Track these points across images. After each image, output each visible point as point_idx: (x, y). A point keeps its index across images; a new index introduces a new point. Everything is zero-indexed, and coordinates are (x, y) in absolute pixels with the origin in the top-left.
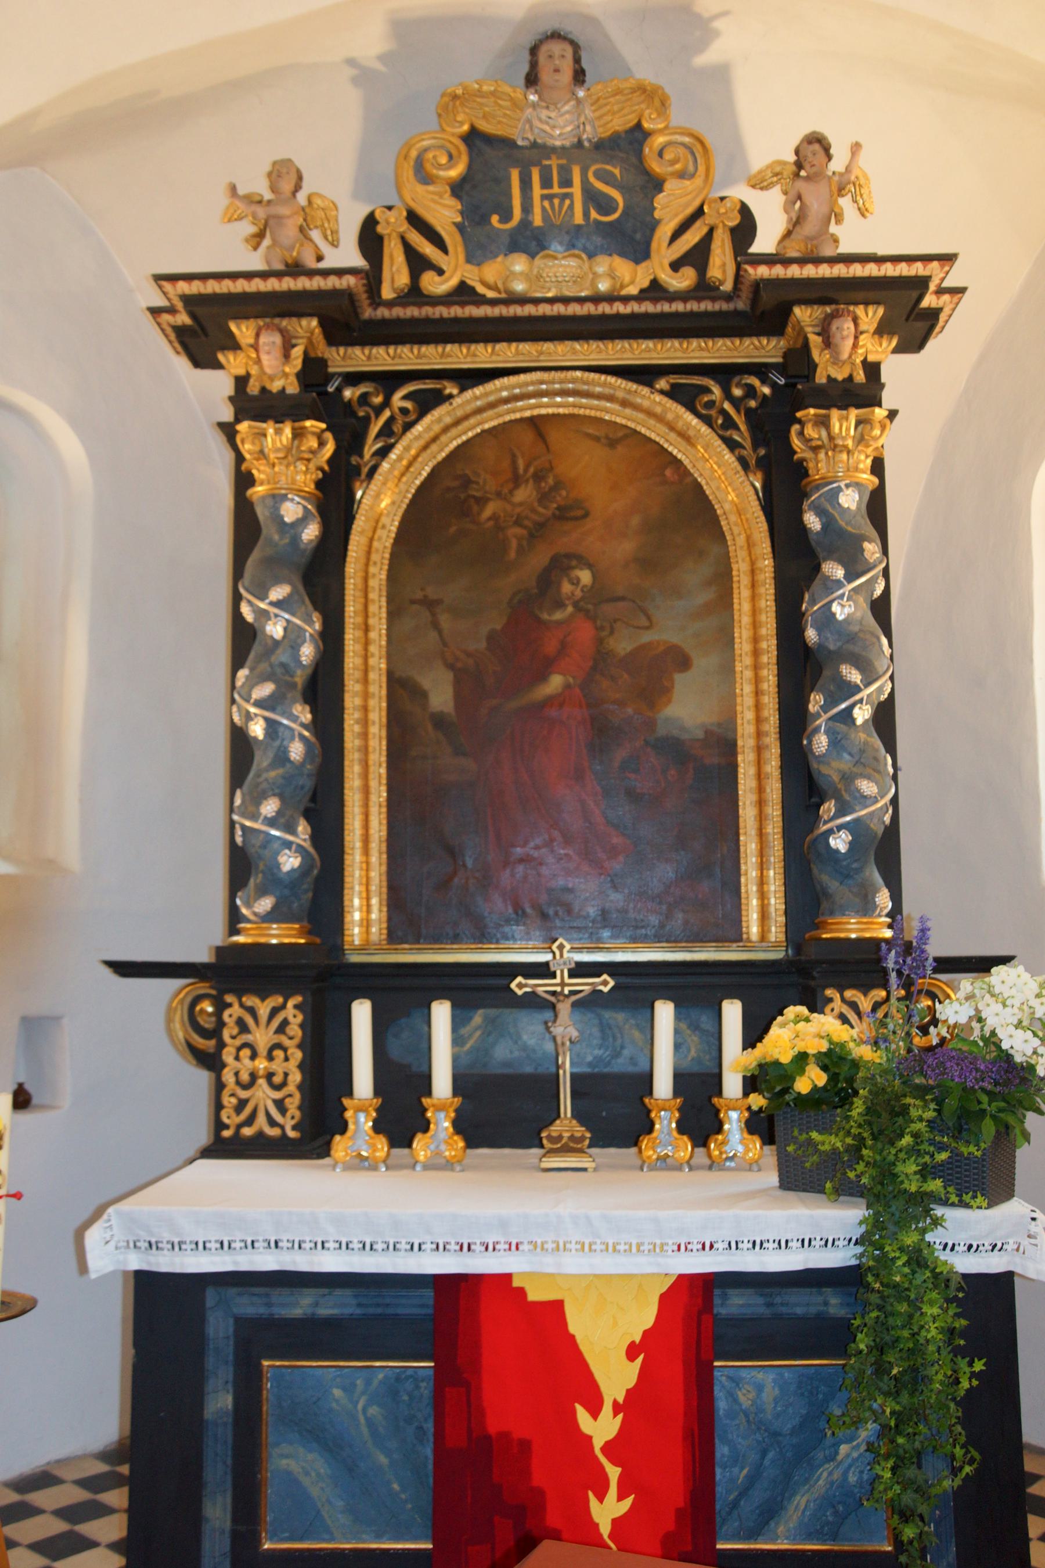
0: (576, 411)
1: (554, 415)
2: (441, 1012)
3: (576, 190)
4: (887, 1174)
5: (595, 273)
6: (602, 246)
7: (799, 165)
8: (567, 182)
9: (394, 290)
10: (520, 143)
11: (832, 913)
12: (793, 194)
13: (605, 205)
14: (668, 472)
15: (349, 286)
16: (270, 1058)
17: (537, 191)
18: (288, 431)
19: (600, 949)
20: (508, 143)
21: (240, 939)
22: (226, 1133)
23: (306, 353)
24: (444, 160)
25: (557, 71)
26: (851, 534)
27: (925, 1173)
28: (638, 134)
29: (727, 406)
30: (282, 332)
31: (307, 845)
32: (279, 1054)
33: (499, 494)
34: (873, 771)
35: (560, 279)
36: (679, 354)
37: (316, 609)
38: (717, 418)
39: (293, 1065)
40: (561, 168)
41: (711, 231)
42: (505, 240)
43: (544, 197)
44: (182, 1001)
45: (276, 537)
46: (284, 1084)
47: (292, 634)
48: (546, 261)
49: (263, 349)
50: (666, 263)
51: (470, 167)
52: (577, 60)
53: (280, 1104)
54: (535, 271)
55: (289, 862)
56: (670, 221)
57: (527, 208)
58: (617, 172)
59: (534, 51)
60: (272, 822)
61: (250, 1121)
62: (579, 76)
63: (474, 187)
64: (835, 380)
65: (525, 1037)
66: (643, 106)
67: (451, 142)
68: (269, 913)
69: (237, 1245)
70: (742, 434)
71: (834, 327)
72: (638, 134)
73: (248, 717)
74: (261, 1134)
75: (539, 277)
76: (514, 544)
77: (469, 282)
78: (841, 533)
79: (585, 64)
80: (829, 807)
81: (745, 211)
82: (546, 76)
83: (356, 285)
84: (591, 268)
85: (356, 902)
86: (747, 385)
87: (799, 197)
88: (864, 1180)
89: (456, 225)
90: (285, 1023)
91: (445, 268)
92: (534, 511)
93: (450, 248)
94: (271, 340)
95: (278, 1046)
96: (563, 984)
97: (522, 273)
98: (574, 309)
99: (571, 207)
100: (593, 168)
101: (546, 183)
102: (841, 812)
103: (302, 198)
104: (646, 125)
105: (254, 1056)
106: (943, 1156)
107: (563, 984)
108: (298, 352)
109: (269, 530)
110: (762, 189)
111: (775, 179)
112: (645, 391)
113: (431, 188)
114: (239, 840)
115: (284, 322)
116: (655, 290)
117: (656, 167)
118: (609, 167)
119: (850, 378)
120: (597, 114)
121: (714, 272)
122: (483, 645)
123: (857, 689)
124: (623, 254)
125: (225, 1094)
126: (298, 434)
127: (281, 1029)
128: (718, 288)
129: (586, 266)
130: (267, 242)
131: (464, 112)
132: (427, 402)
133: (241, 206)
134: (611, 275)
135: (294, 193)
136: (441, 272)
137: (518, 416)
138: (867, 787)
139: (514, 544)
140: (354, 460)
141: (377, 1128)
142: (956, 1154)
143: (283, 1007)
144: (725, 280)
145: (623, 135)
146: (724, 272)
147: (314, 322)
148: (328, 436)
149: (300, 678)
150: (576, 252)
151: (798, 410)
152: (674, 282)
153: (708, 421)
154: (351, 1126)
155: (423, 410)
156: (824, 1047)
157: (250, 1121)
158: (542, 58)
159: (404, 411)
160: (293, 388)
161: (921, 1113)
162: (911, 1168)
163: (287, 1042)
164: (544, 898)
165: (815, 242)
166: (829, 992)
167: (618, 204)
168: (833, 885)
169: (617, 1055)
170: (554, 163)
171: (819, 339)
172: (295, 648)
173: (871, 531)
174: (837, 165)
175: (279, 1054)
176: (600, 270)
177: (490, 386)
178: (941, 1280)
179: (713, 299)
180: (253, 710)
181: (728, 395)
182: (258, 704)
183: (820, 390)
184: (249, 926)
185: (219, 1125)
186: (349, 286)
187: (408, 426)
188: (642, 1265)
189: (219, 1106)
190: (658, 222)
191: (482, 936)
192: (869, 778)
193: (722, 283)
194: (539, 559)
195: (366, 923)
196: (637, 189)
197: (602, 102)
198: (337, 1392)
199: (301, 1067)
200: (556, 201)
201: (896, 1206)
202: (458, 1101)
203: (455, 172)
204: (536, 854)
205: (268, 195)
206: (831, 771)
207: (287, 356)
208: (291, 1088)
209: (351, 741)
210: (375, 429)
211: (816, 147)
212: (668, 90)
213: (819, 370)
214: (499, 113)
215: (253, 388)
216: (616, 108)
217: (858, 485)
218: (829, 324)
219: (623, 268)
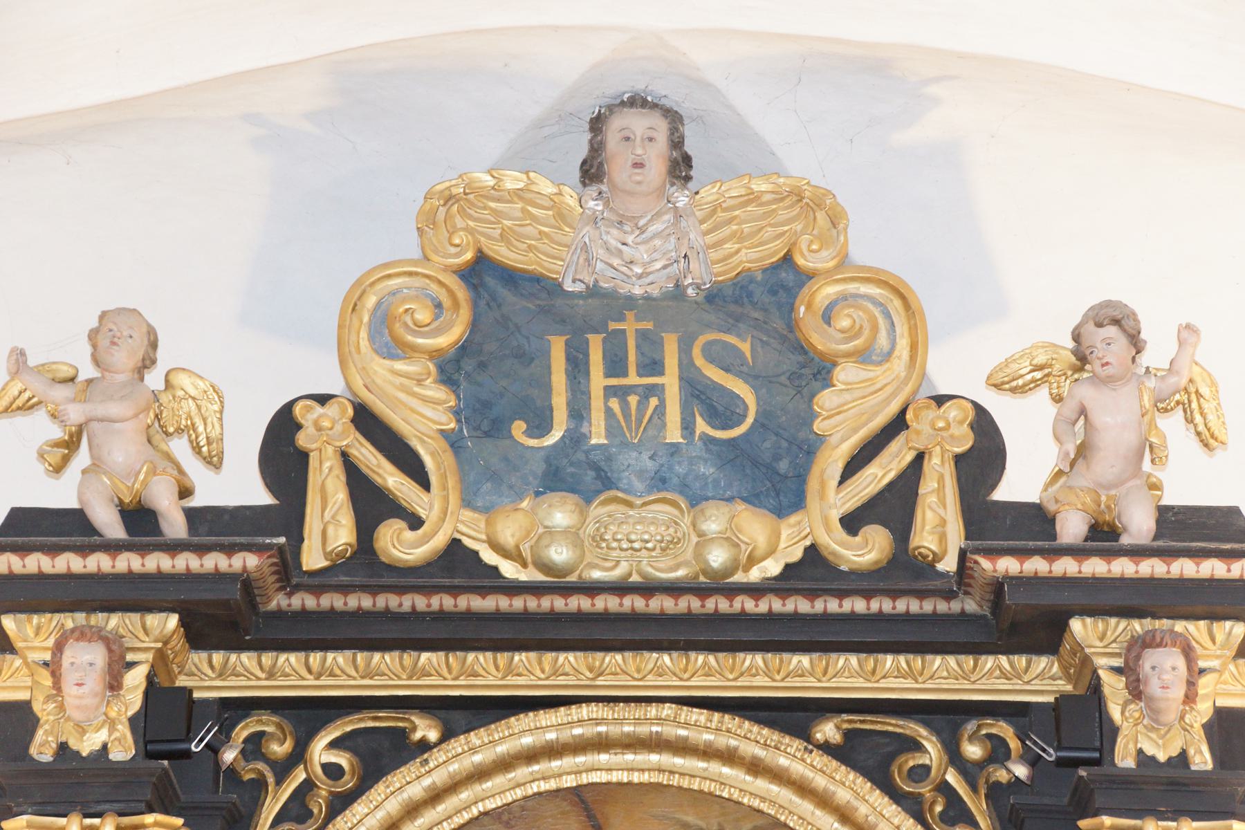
0: (663, 779)
1: (620, 784)
3: (670, 381)
5: (701, 534)
6: (716, 482)
7: (1082, 359)
8: (653, 366)
9: (327, 555)
10: (569, 286)
12: (1070, 408)
15: (245, 568)
17: (598, 380)
23: (150, 679)
24: (423, 316)
25: (638, 165)
29: (952, 777)
35: (636, 545)
36: (860, 682)
38: (933, 803)
40: (643, 335)
41: (920, 458)
42: (539, 467)
43: (610, 391)
48: (611, 508)
49: (69, 678)
50: (835, 515)
51: (474, 325)
52: (677, 143)
54: (590, 529)
56: (843, 440)
57: (578, 412)
58: (745, 347)
59: (597, 124)
63: (482, 366)
66: (798, 227)
67: (440, 283)
75: (598, 539)
77: (467, 542)
79: (689, 148)
81: (983, 423)
83: (259, 568)
84: (694, 525)
86: (990, 736)
87: (1083, 412)
91: (422, 513)
93: (434, 479)
97: (566, 532)
98: (662, 604)
99: (661, 410)
100: (702, 340)
101: (615, 366)
103: (154, 380)
104: (800, 261)
108: (136, 679)
110: (1013, 390)
111: (1038, 375)
112: (796, 745)
113: (399, 366)
115: (114, 621)
117: (820, 339)
118: (731, 339)
120: (710, 239)
121: (924, 539)
124: (753, 499)
128: (932, 566)
129: (687, 520)
130: (82, 458)
131: (467, 229)
136: (415, 522)
137: (552, 785)
144: (945, 552)
145: (759, 277)
146: (943, 538)
147: (173, 620)
150: (669, 496)
151: (1083, 817)
152: (848, 554)
155: (372, 773)
159: (333, 771)
160: (123, 751)
165: (1113, 492)
167: (746, 408)
170: (630, 326)
174: (1156, 354)
176: (712, 526)
177: (499, 730)
179: (921, 595)
181: (955, 757)
183: (1125, 781)
186: (245, 568)
193: (937, 558)
196: (783, 379)
197: (721, 215)
200: (633, 400)
203: (444, 341)
205: (87, 371)
207: (114, 685)
211: (1112, 331)
212: (844, 199)
213: (1120, 741)
214: (529, 230)
216: (746, 228)
218: (1138, 657)
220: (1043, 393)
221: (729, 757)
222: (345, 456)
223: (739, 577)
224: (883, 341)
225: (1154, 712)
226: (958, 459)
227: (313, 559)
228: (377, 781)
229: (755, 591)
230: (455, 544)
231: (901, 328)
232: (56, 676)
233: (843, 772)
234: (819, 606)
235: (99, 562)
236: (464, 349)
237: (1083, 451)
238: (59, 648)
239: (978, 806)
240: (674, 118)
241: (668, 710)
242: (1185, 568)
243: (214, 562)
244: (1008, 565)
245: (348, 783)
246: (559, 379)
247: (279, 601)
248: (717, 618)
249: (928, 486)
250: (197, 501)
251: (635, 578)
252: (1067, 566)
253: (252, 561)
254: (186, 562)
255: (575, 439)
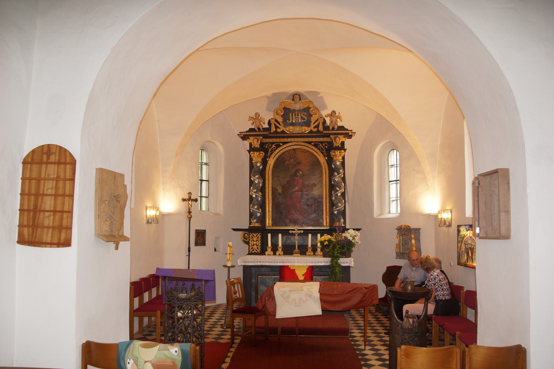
2: (280, 235)
3: (300, 117)
4: (334, 254)
8: (298, 115)
11: (335, 222)
13: (304, 119)
14: (313, 157)
16: (256, 242)
17: (294, 117)
18: (258, 153)
19: (303, 227)
20: (289, 109)
21: (252, 225)
22: (250, 252)
24: (280, 112)
26: (338, 168)
27: (338, 253)
28: (309, 108)
29: (322, 147)
30: (257, 139)
31: (261, 212)
32: (257, 241)
33: (288, 160)
34: (341, 202)
37: (262, 178)
39: (259, 243)
40: (297, 113)
41: (319, 122)
43: (295, 118)
44: (243, 234)
45: (256, 168)
46: (258, 245)
47: (259, 183)
51: (284, 113)
52: (300, 97)
53: (257, 248)
55: (259, 215)
58: (306, 114)
59: (293, 96)
60: (256, 209)
61: (253, 250)
62: (300, 99)
64: (336, 146)
65: (292, 240)
68: (256, 222)
69: (256, 262)
70: (325, 151)
71: (336, 139)
72: (309, 108)
73: (253, 194)
74: (255, 252)
76: (291, 168)
78: (337, 168)
80: (334, 207)
81: (324, 120)
82: (295, 100)
85: (267, 220)
88: (331, 255)
89: (282, 121)
90: (258, 237)
92: (294, 163)
94: (256, 140)
95: (257, 240)
96: (296, 232)
99: (299, 119)
101: (295, 116)
102: (336, 208)
103: (259, 118)
105: (254, 242)
106: (340, 251)
107: (296, 232)
108: (259, 141)
109: (255, 167)
112: (310, 145)
114: (251, 211)
116: (311, 132)
119: (339, 146)
121: (320, 129)
122: (286, 183)
123: (338, 191)
124: (306, 126)
125: (250, 246)
126: (259, 154)
127: (258, 238)
129: (301, 128)
130: (254, 124)
132: (278, 146)
133: (251, 119)
134: (304, 129)
135: (258, 117)
136: (280, 128)
138: (339, 205)
139: (291, 168)
140: (267, 155)
141: (271, 250)
142: (341, 251)
143: (258, 235)
147: (262, 137)
148: (264, 153)
149: (260, 188)
153: (319, 149)
154: (268, 250)
156: (328, 239)
157: (253, 250)
158: (295, 97)
161: (338, 246)
162: (336, 253)
163: (258, 240)
164: (294, 220)
166: (334, 233)
168: (335, 218)
169: (305, 242)
170: (296, 112)
171: (334, 140)
172: (259, 184)
173: (342, 167)
175: (257, 241)
178: (339, 265)
180: (253, 193)
182: (254, 192)
184: (50, 235)
185: (249, 251)
187: (275, 150)
188: (305, 264)
189: (249, 248)
190: (312, 121)
191: (286, 225)
192: (340, 203)
194: (294, 170)
195: (269, 223)
198: (268, 280)
199: (260, 243)
201: (335, 257)
202: (282, 247)
203: (282, 114)
204: (293, 213)
205: (255, 117)
206: (335, 202)
207: (258, 142)
208: (259, 246)
209: (267, 197)
210: (270, 150)
211: (334, 113)
215: (253, 147)
217: (339, 161)
219: (306, 128)
220: (329, 117)
221: (305, 146)
222: (274, 123)
223: (305, 133)
224: (316, 113)
225: (336, 142)
226: (322, 122)
227: (272, 132)
228: (291, 245)
229: (306, 134)
230: (283, 130)
231: (318, 112)
232: (254, 141)
233: (314, 147)
234: (311, 135)
235: (256, 133)
236: (283, 114)
237: (332, 122)
238: (254, 139)
239: (324, 149)
240: (299, 95)
241: (300, 143)
242: (339, 132)
243: (265, 133)
244: (325, 132)
245: (275, 148)
246: (291, 117)
247: (269, 135)
248: (303, 136)
249: (320, 124)
250: (263, 127)
251: (297, 133)
252: (330, 132)
253: (267, 133)
254: (262, 133)
255: (292, 121)
